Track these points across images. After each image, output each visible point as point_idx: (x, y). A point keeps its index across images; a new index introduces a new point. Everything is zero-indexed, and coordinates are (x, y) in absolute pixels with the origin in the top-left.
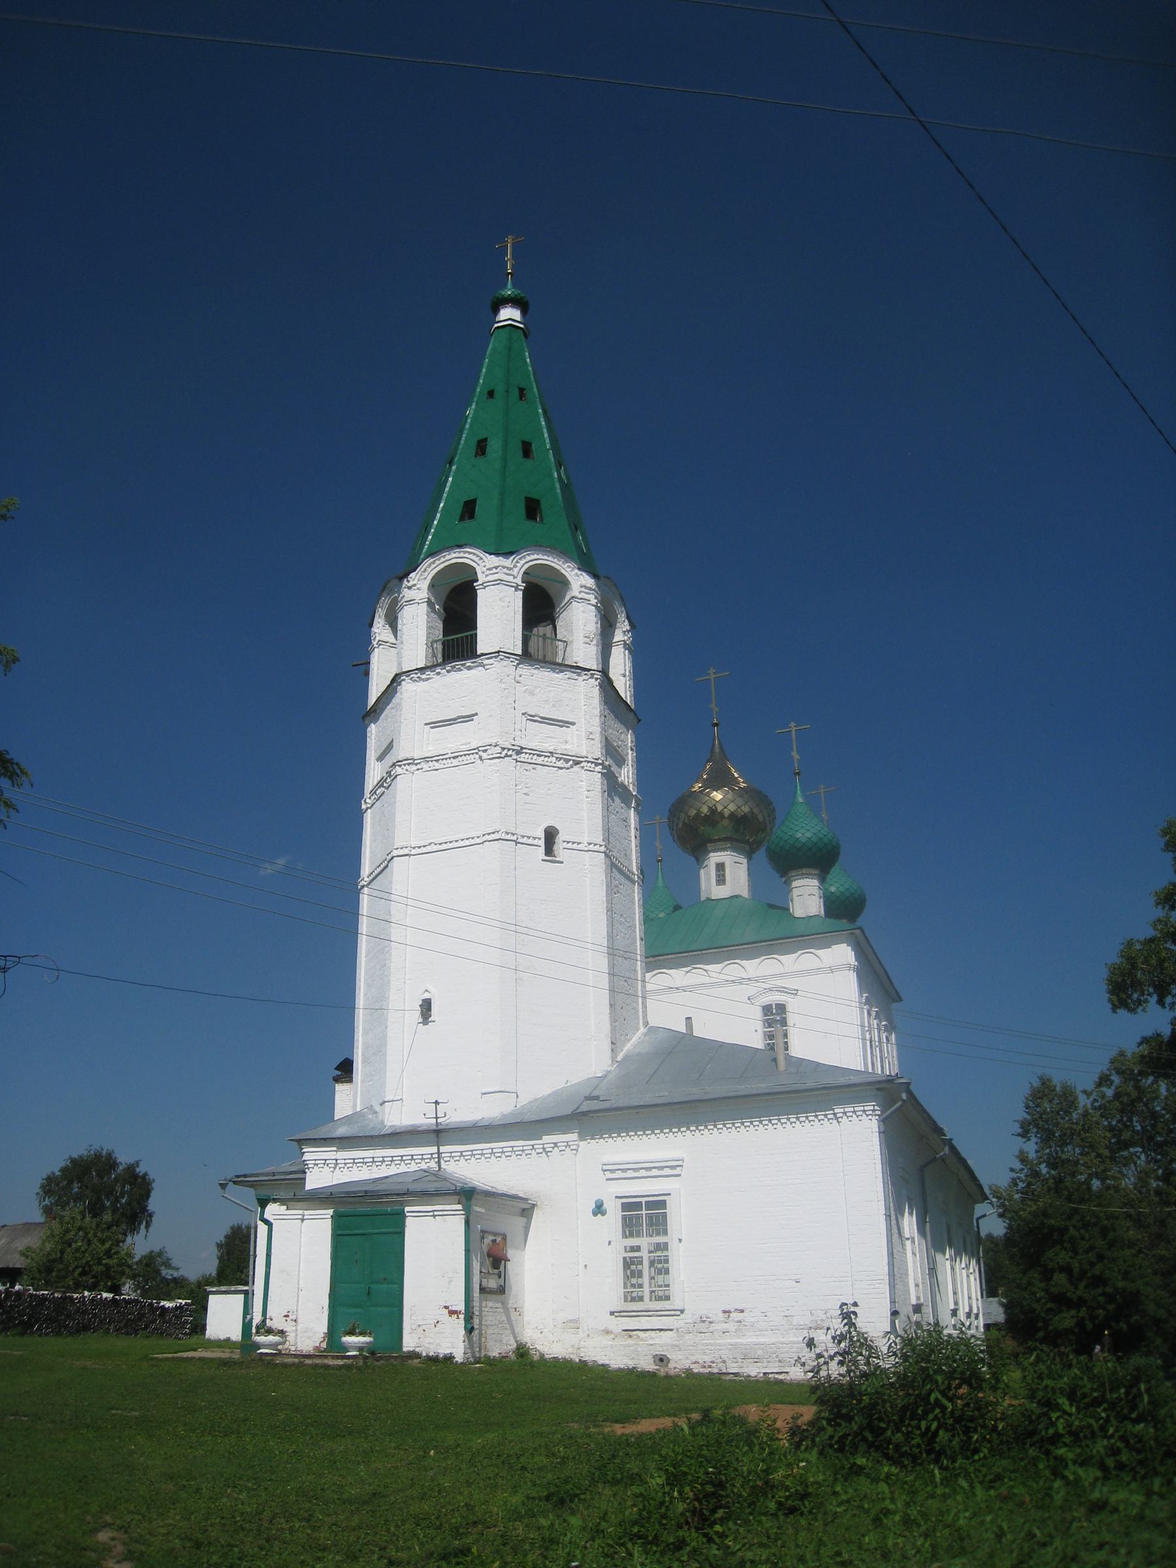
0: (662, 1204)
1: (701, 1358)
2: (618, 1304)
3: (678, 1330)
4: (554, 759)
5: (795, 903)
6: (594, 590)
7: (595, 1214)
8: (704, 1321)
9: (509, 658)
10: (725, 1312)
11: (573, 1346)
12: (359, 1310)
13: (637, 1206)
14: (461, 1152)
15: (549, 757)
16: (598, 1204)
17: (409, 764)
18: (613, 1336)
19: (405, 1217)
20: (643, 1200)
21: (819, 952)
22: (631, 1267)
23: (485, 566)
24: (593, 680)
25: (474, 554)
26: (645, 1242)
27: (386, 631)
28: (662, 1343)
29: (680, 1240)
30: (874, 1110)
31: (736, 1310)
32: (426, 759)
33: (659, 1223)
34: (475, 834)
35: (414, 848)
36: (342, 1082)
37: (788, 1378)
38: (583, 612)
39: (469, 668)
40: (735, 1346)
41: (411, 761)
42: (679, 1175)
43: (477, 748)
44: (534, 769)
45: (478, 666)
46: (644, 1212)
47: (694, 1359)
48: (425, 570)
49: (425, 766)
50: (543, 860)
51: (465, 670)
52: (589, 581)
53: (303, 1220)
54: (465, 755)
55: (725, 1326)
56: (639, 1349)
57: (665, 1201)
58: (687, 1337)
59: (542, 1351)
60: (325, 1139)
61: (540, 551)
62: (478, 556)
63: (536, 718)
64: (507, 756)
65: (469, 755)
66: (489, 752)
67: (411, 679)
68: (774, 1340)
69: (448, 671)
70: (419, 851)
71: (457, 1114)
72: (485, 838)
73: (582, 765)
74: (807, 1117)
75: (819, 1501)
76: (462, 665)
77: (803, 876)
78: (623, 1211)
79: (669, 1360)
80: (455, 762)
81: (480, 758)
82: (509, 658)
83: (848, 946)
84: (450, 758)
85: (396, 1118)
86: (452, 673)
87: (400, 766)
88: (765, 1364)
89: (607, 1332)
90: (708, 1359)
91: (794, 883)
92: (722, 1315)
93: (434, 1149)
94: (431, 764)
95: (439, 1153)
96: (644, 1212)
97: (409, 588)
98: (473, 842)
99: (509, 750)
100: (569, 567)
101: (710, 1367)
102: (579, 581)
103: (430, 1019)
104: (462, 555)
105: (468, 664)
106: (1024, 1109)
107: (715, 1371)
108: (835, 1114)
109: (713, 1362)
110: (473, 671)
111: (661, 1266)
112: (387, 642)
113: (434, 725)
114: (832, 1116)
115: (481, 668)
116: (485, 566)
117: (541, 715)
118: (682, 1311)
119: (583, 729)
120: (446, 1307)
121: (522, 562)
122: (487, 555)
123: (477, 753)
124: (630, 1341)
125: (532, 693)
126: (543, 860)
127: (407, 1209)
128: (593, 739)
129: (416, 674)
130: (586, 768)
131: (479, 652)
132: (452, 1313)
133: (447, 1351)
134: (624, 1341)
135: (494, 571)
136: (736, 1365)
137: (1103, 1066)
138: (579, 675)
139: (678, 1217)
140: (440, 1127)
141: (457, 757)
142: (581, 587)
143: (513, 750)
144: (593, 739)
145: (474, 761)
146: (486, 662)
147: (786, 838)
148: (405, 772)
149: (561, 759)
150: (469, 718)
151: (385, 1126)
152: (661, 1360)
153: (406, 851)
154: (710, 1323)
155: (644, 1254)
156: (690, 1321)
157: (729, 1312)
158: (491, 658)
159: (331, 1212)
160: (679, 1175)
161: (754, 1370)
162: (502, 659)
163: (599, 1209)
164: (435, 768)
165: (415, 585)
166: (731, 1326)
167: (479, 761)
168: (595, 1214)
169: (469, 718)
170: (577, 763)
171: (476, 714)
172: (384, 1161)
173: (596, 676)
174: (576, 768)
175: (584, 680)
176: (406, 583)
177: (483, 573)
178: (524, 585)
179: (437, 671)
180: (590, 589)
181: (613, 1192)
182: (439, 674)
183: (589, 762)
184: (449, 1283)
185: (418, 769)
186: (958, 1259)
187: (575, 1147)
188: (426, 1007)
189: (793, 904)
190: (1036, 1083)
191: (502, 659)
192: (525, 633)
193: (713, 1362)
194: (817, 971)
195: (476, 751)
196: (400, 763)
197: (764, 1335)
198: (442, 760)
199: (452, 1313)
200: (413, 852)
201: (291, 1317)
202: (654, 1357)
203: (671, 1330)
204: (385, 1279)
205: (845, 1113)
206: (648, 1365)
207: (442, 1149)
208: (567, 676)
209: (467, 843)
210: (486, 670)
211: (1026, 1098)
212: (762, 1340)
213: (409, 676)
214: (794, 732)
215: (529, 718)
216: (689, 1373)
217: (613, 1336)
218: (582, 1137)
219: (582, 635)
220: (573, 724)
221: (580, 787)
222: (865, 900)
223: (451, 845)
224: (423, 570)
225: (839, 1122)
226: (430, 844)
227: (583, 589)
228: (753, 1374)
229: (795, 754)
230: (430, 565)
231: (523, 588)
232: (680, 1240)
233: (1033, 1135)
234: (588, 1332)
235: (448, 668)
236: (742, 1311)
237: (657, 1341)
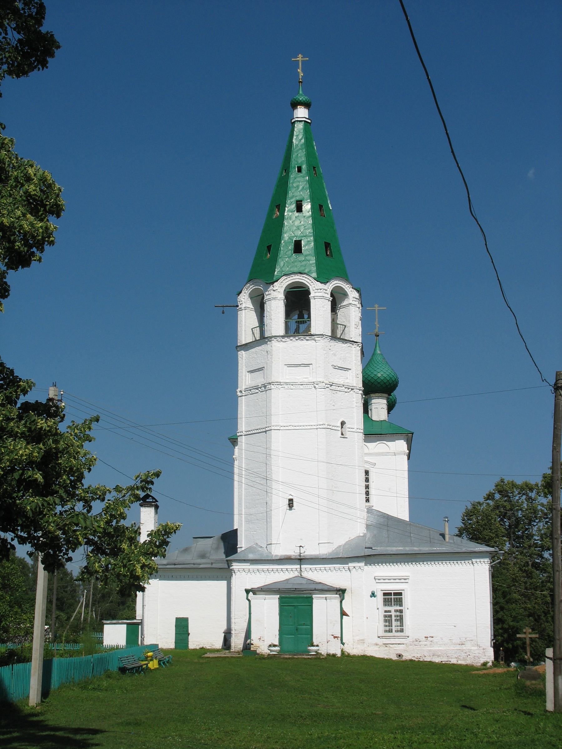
0: (400, 594)
1: (416, 655)
2: (381, 633)
3: (406, 644)
4: (344, 388)
5: (373, 411)
6: (358, 299)
7: (371, 597)
8: (417, 641)
9: (327, 338)
10: (425, 637)
11: (362, 650)
12: (293, 636)
14: (311, 568)
15: (342, 387)
16: (373, 593)
17: (278, 385)
18: (379, 646)
19: (313, 599)
20: (392, 592)
21: (388, 443)
22: (388, 619)
23: (314, 287)
24: (358, 347)
25: (308, 279)
26: (392, 609)
27: (248, 301)
28: (400, 649)
29: (408, 609)
30: (488, 562)
31: (430, 637)
32: (286, 383)
33: (399, 602)
34: (312, 424)
35: (282, 426)
36: (145, 507)
37: (451, 663)
38: (354, 312)
39: (307, 340)
40: (430, 651)
41: (279, 383)
42: (408, 582)
43: (314, 382)
44: (336, 393)
45: (312, 340)
46: (393, 597)
47: (413, 655)
48: (282, 282)
49: (286, 387)
50: (341, 437)
51: (305, 341)
52: (357, 295)
53: (265, 599)
54: (307, 384)
55: (426, 643)
56: (390, 651)
57: (401, 593)
58: (410, 647)
59: (348, 652)
60: (244, 560)
61: (337, 279)
62: (310, 280)
63: (336, 367)
64: (327, 387)
65: (309, 384)
66: (320, 385)
67: (277, 340)
68: (445, 649)
69: (297, 340)
70: (285, 428)
71: (310, 551)
72: (318, 427)
73: (354, 390)
74: (461, 562)
76: (304, 338)
77: (378, 397)
78: (384, 596)
79: (403, 656)
80: (301, 387)
81: (315, 387)
82: (327, 338)
83: (404, 441)
84: (299, 385)
85: (278, 551)
86: (298, 341)
87: (273, 385)
88: (442, 658)
89: (377, 645)
90: (419, 655)
91: (373, 400)
92: (424, 638)
93: (299, 566)
94: (289, 386)
95: (301, 568)
96: (393, 597)
97: (274, 291)
98: (312, 427)
99: (328, 384)
100: (348, 287)
101: (419, 658)
102: (353, 294)
103: (293, 508)
104: (301, 278)
105: (307, 338)
106: (461, 521)
107: (421, 660)
108: (472, 562)
109: (421, 657)
110: (309, 342)
112: (249, 308)
113: (290, 366)
114: (471, 563)
115: (313, 341)
116: (314, 287)
117: (338, 366)
118: (408, 637)
119: (354, 372)
120: (332, 635)
121: (331, 285)
122: (316, 281)
123: (313, 384)
124: (386, 648)
125: (335, 355)
126: (341, 437)
127: (314, 596)
128: (358, 378)
129: (280, 338)
130: (356, 392)
131: (313, 331)
132: (335, 637)
133: (334, 652)
134: (384, 648)
135: (319, 291)
136: (430, 658)
137: (491, 488)
138: (353, 344)
139: (407, 599)
140: (302, 557)
141: (302, 385)
142: (353, 298)
143: (330, 385)
144: (358, 378)
145: (311, 388)
146: (316, 339)
147: (372, 376)
148: (276, 388)
149: (346, 388)
150: (308, 365)
151: (273, 555)
152: (400, 656)
153: (278, 428)
154: (420, 641)
155: (393, 614)
156: (411, 641)
157: (427, 637)
158: (319, 337)
159: (278, 596)
160: (408, 582)
161: (437, 660)
162: (324, 339)
163: (373, 595)
164: (291, 388)
165: (277, 290)
166: (428, 643)
167: (314, 388)
168: (371, 597)
169: (308, 365)
170: (352, 389)
171: (312, 364)
172: (273, 570)
173: (359, 345)
174: (352, 392)
175: (355, 347)
176: (272, 288)
177: (314, 290)
178: (332, 298)
179: (291, 339)
180: (357, 299)
181: (380, 588)
182: (291, 340)
183: (357, 389)
184: (334, 626)
185: (282, 387)
186: (113, 646)
188: (291, 503)
189: (371, 412)
190: (470, 507)
191: (324, 339)
193: (421, 657)
194: (387, 454)
195: (313, 383)
196: (273, 384)
197: (441, 647)
198: (295, 385)
199: (335, 637)
200: (282, 428)
201: (262, 639)
202: (397, 654)
203: (403, 644)
204: (304, 624)
205: (476, 562)
206: (395, 658)
207: (302, 566)
208: (348, 346)
209: (309, 427)
210: (316, 343)
211: (463, 515)
212: (440, 648)
213: (276, 338)
214: (377, 310)
215: (334, 367)
216: (411, 661)
217: (379, 646)
218: (366, 565)
219: (354, 324)
220: (350, 369)
221: (353, 401)
222: (395, 403)
223: (301, 428)
224: (281, 282)
225: (473, 565)
226: (290, 426)
227: (354, 299)
228: (437, 661)
229: (376, 323)
230: (284, 280)
231: (331, 300)
232: (408, 609)
233: (465, 536)
234: (368, 645)
235: (296, 338)
236: (433, 637)
237: (398, 648)
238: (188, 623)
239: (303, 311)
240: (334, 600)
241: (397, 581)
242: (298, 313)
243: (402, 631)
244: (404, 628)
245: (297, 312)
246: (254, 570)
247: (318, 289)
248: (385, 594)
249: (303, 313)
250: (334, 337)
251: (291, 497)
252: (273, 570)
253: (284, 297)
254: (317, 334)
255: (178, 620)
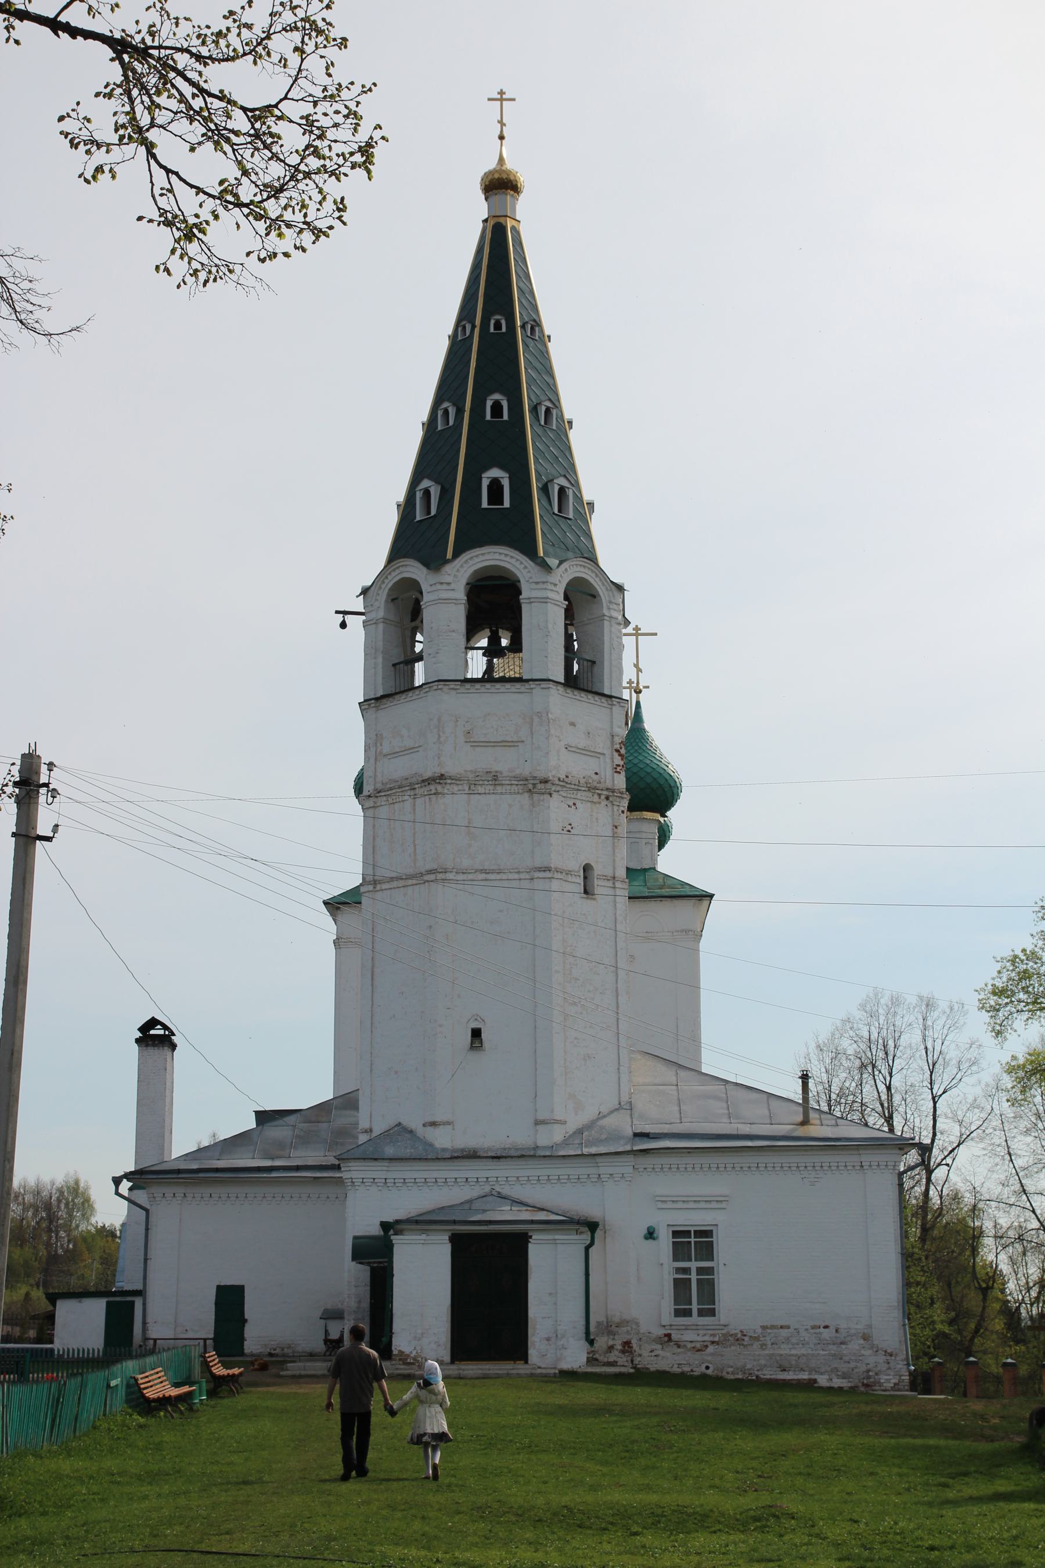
7: (646, 1238)
13: (687, 1233)
16: (651, 1230)
20: (692, 1229)
22: (681, 1286)
46: (693, 1240)
57: (711, 1231)
75: (623, 1521)
96: (693, 1240)
111: (708, 1289)
163: (650, 1234)
178: (567, 603)
181: (666, 1221)
186: (61, 1353)
187: (630, 1179)
192: (568, 655)
238: (243, 1297)
239: (500, 631)
240: (571, 1245)
241: (703, 1205)
242: (489, 634)
243: (712, 1313)
244: (716, 1306)
245: (487, 632)
246: (791, 1165)
247: (537, 583)
248: (676, 1234)
249: (500, 634)
250: (572, 682)
251: (475, 1025)
252: (528, 1180)
253: (466, 598)
254: (535, 677)
255: (221, 1290)
